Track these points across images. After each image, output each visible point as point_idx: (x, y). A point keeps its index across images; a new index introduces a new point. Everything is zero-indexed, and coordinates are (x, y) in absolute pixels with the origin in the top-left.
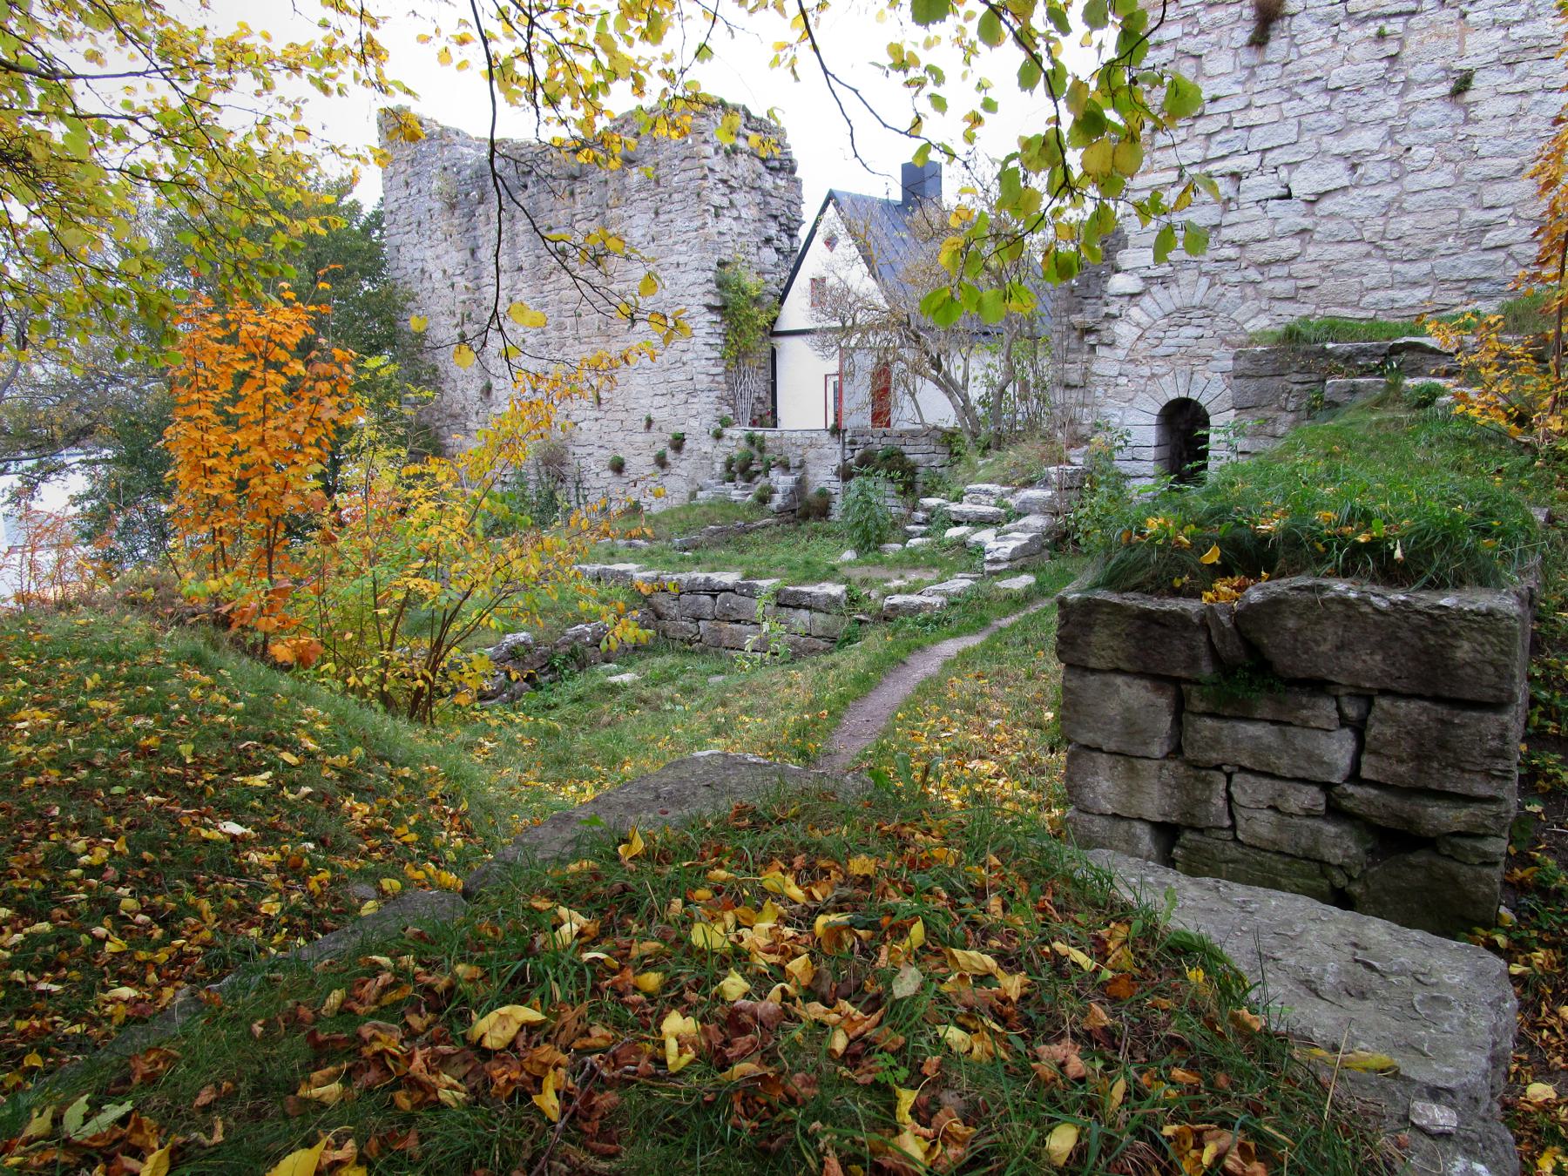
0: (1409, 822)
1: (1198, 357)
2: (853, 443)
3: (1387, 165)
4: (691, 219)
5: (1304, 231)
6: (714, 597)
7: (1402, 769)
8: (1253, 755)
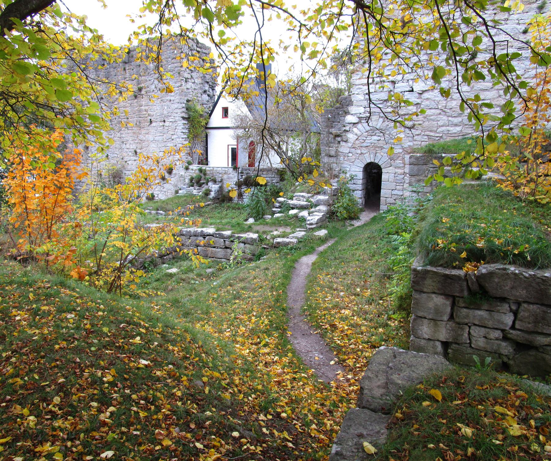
0: (531, 342)
1: (378, 147)
2: (242, 173)
3: (447, 83)
4: (176, 83)
5: (417, 104)
6: (204, 238)
7: (530, 326)
8: (480, 321)
